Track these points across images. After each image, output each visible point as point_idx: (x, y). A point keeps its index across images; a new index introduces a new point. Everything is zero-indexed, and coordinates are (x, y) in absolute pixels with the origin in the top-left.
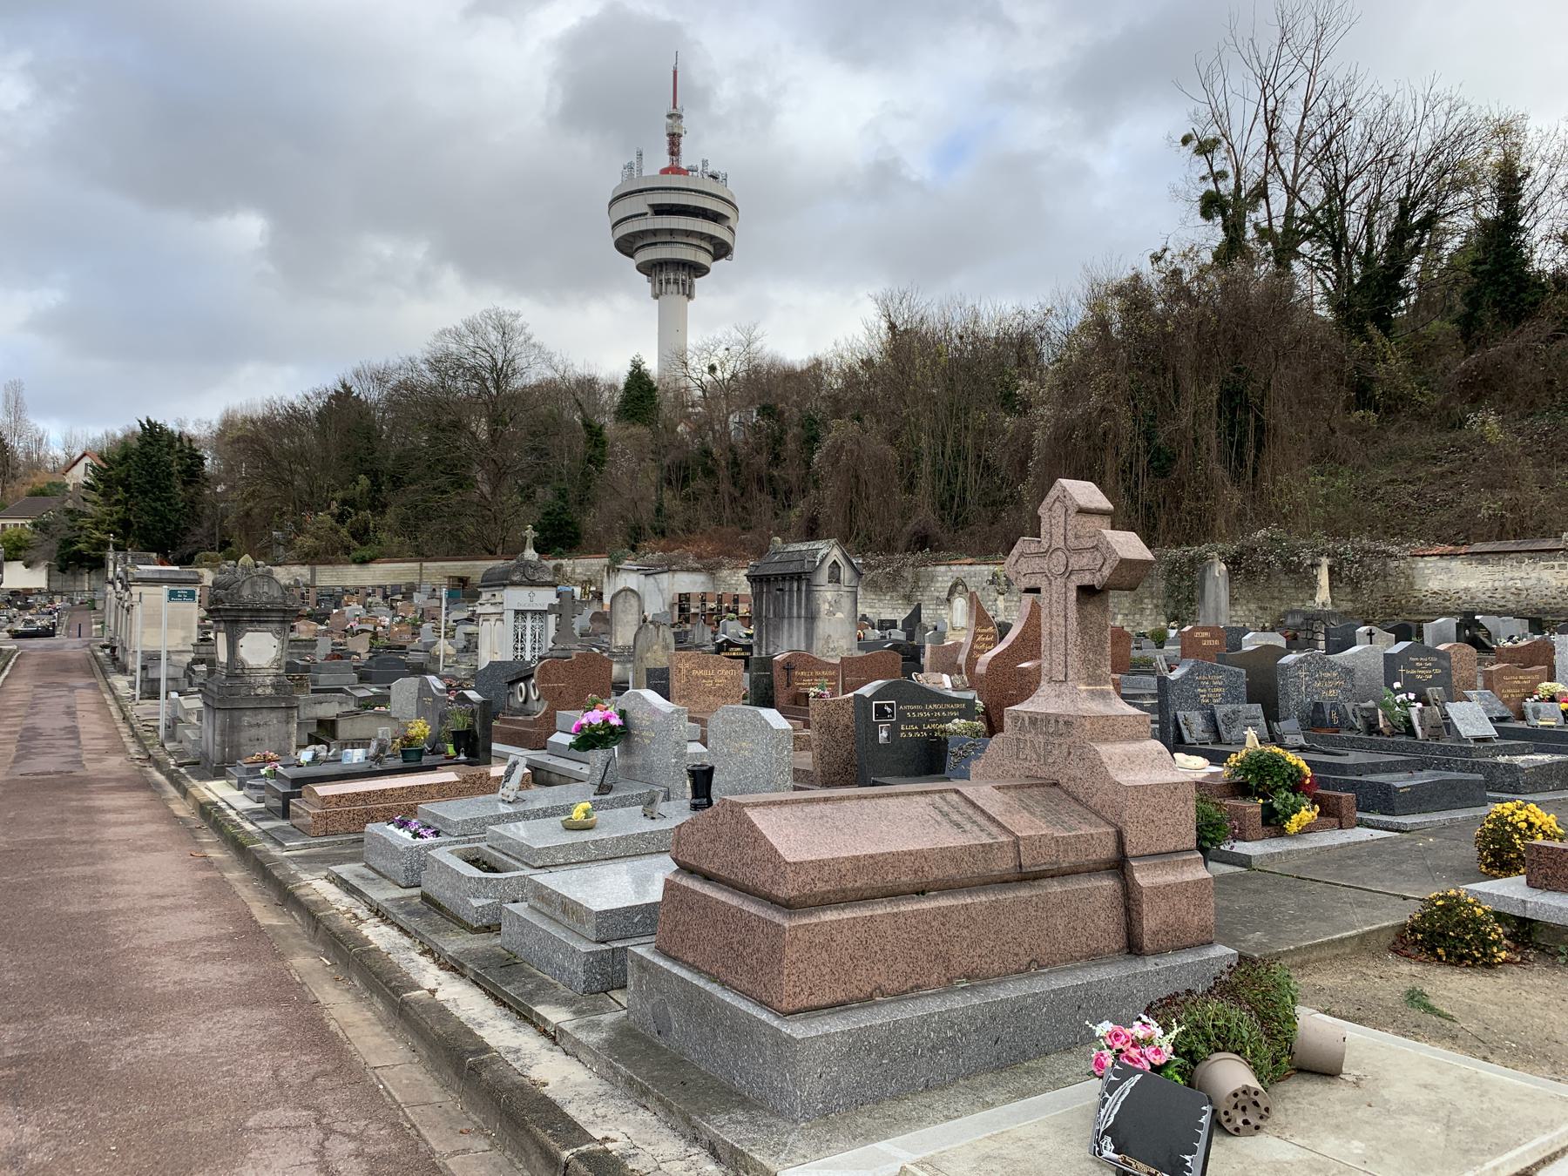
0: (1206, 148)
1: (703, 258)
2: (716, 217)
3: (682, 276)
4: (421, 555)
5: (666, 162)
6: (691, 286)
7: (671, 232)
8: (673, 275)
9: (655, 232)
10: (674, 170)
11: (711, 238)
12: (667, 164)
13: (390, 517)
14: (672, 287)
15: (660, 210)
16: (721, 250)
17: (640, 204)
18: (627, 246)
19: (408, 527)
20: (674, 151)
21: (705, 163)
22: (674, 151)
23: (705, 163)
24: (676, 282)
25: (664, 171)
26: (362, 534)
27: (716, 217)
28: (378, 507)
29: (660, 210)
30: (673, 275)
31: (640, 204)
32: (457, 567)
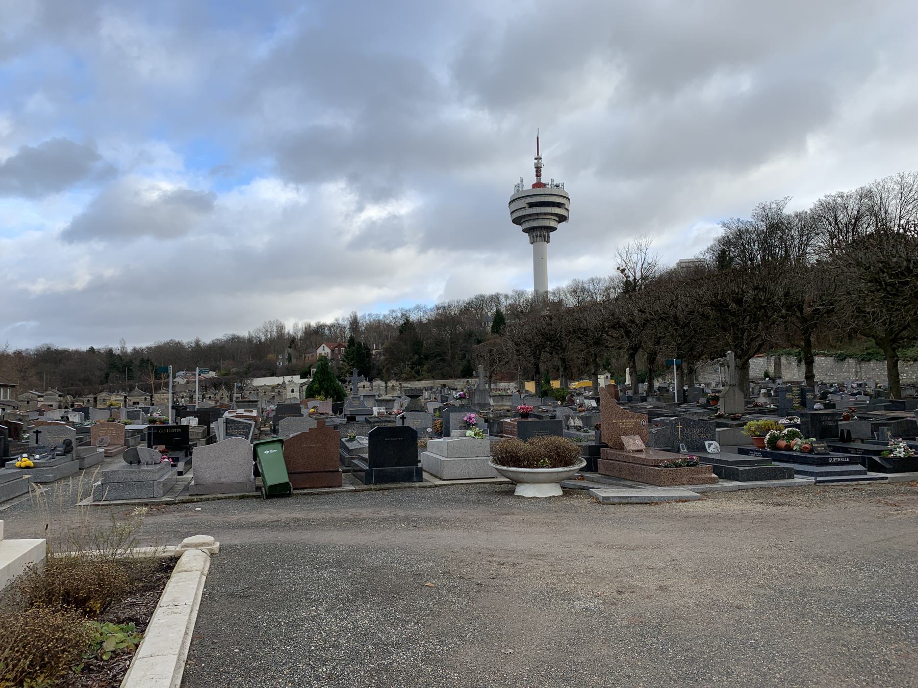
0: (623, 271)
1: (553, 224)
2: (558, 205)
3: (544, 233)
4: (434, 378)
5: (535, 181)
6: (548, 237)
7: (537, 214)
8: (539, 233)
9: (530, 215)
10: (538, 185)
11: (557, 215)
12: (535, 181)
13: (425, 367)
14: (539, 239)
15: (532, 205)
16: (562, 219)
17: (522, 203)
18: (517, 221)
19: (429, 371)
20: (538, 174)
21: (552, 180)
22: (538, 174)
23: (552, 180)
24: (541, 236)
25: (534, 186)
26: (418, 373)
27: (558, 205)
28: (422, 364)
29: (532, 205)
30: (539, 233)
31: (522, 203)
32: (443, 382)
